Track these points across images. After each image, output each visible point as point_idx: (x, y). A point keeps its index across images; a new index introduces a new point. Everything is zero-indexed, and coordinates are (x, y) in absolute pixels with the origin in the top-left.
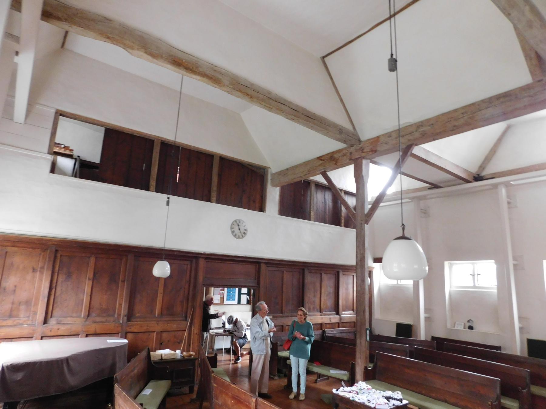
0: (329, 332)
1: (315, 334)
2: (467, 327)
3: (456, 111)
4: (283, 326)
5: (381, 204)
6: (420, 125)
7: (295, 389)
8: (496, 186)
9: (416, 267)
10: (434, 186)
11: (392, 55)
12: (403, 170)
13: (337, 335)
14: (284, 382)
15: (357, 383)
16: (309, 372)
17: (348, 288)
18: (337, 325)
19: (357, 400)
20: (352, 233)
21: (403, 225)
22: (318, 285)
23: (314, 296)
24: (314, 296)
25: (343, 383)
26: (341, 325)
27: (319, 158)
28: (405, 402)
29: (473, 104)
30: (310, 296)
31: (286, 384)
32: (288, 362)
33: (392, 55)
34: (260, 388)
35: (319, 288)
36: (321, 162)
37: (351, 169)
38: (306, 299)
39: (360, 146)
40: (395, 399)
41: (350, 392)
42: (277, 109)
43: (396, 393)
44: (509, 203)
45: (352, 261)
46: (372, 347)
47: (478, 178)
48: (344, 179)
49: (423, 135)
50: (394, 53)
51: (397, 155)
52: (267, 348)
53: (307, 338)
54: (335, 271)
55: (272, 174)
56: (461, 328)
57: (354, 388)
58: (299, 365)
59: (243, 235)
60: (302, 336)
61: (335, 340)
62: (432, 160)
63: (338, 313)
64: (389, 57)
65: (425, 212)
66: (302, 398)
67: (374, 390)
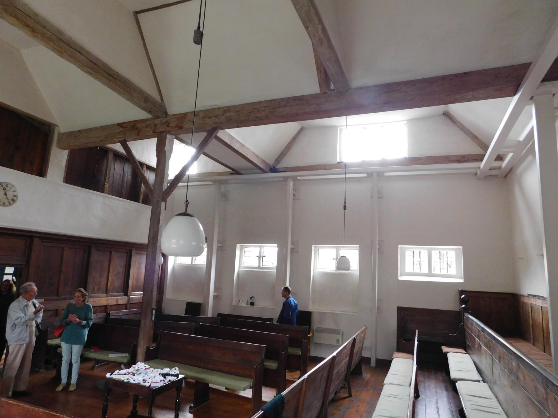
0: (114, 314)
1: (95, 318)
2: (249, 303)
3: (259, 103)
4: (57, 310)
5: (180, 184)
6: (227, 109)
7: (64, 380)
8: (286, 179)
9: (194, 243)
10: (235, 172)
11: (199, 27)
12: (206, 151)
13: (123, 317)
14: (53, 373)
15: (135, 364)
16: (84, 359)
17: (139, 267)
18: (124, 306)
19: (132, 381)
20: (147, 210)
21: (187, 201)
22: (106, 264)
23: (100, 276)
24: (100, 276)
25: (122, 366)
26: (128, 306)
27: (120, 125)
28: (181, 376)
29: (274, 100)
30: (95, 276)
31: (54, 375)
32: (58, 350)
33: (199, 27)
34: (16, 385)
35: (107, 268)
36: (121, 129)
37: (152, 143)
38: (90, 280)
39: (166, 119)
40: (172, 375)
41: (125, 374)
42: (70, 56)
43: (173, 369)
44: (294, 195)
45: (144, 240)
46: (156, 326)
47: (273, 170)
48: (145, 152)
49: (229, 120)
50: (201, 25)
51: (201, 136)
52: (30, 337)
53: (84, 322)
54: (128, 249)
55: (59, 134)
56: (244, 304)
57: (131, 370)
58: (71, 352)
59: (11, 202)
60: (78, 320)
61: (121, 322)
62: (236, 147)
63: (126, 294)
64: (196, 28)
65: (224, 196)
66: (72, 388)
67: (151, 369)
